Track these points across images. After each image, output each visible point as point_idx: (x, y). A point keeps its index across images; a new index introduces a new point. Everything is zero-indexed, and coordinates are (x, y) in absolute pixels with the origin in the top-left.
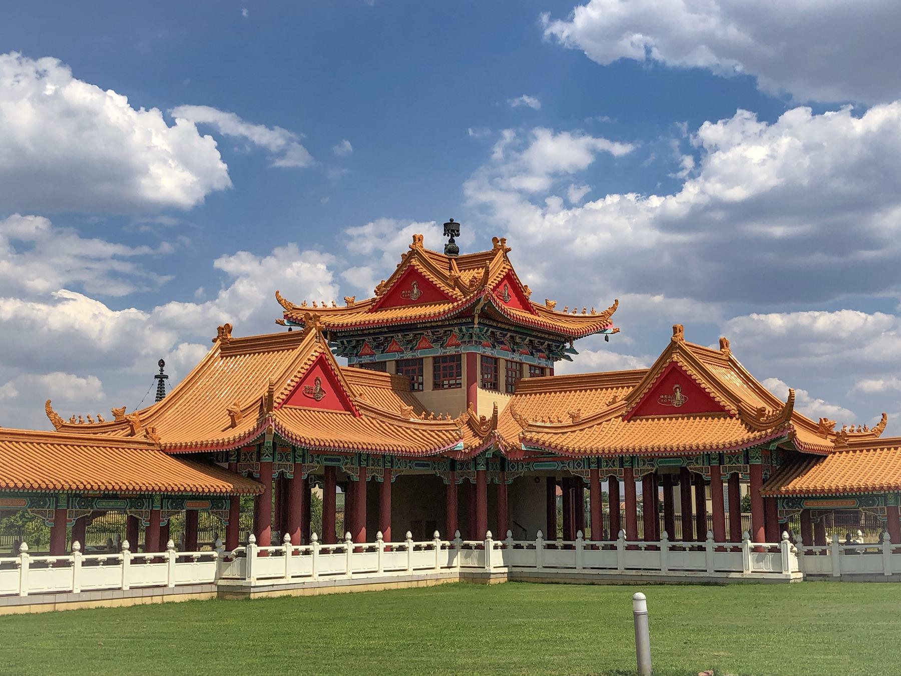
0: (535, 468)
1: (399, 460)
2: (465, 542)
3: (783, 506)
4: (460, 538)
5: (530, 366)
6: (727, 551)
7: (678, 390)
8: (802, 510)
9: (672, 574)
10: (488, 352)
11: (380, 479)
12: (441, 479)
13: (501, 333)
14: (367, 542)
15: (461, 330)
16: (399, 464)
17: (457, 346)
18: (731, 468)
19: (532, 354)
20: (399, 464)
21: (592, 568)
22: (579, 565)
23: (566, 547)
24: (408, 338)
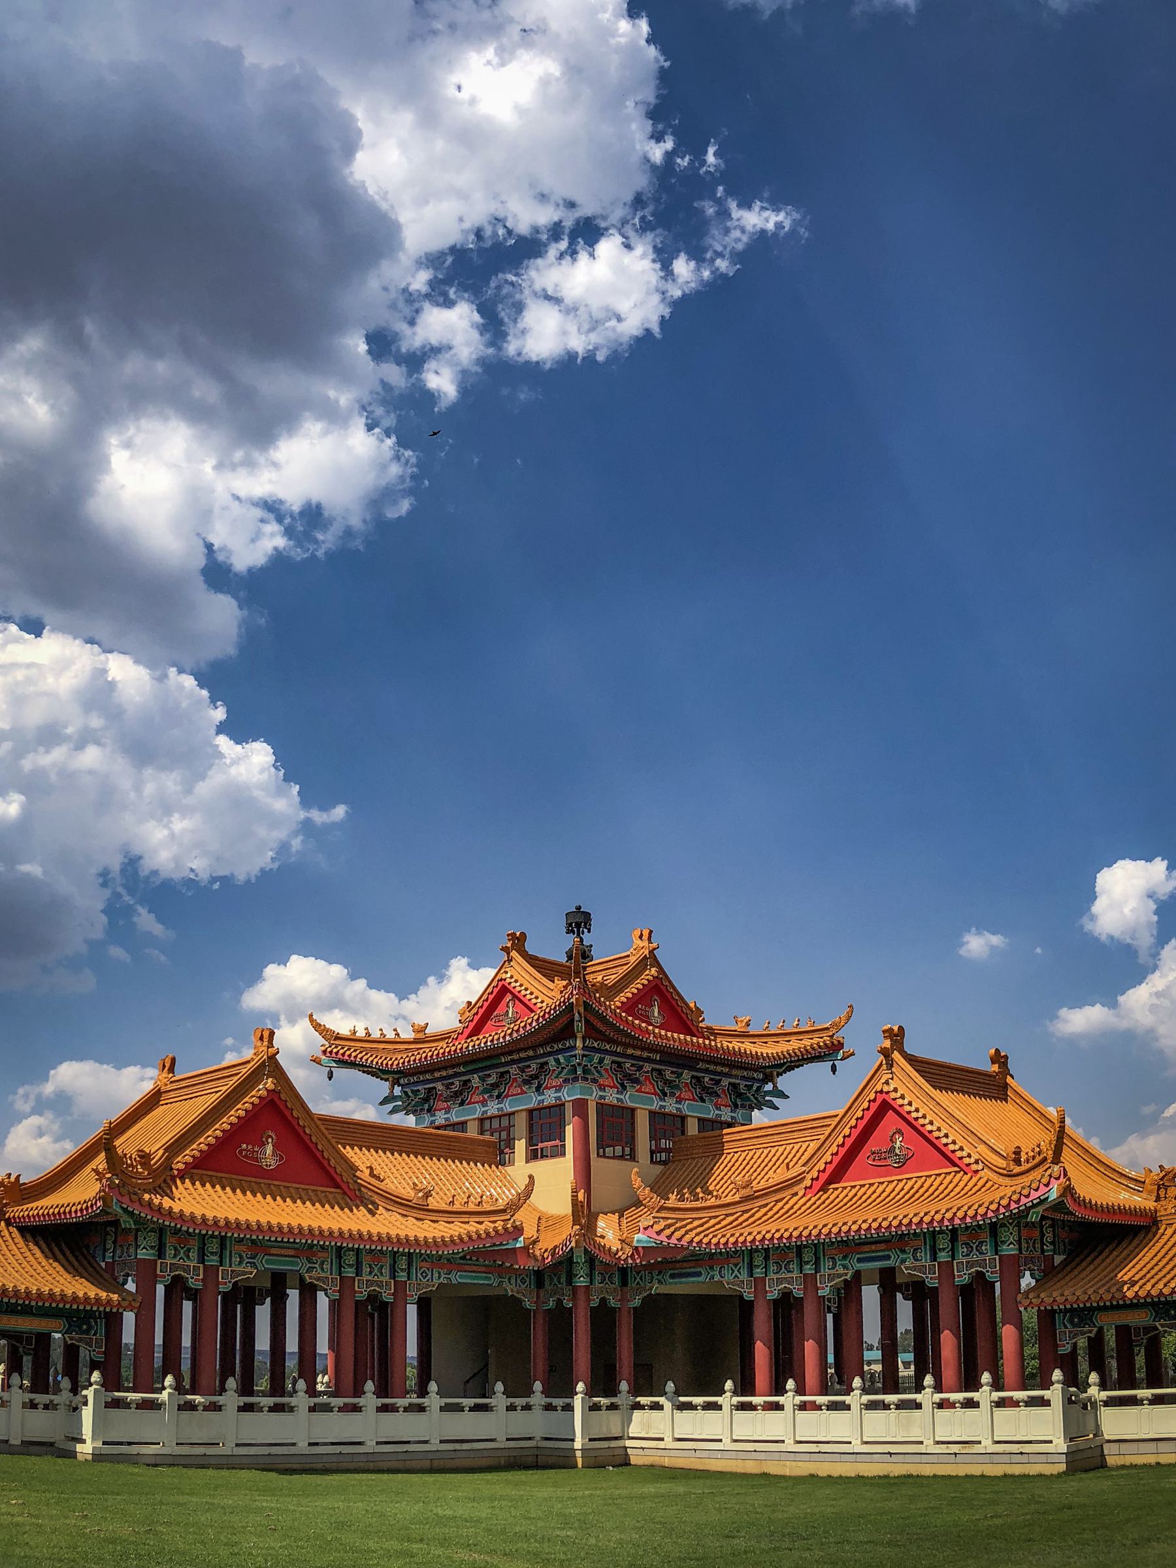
0: (459, 1280)
1: (638, 1273)
2: (595, 1399)
3: (1064, 1323)
4: (503, 1394)
5: (700, 1119)
6: (516, 1410)
7: (270, 1140)
8: (1095, 1329)
9: (512, 1444)
10: (611, 1097)
11: (613, 1303)
12: (520, 1301)
13: (632, 1065)
14: (1024, 1388)
15: (557, 1061)
16: (638, 1279)
17: (558, 1088)
18: (970, 1264)
19: (703, 1101)
20: (638, 1279)
21: (333, 1444)
22: (538, 1434)
23: (277, 1408)
24: (491, 1080)
